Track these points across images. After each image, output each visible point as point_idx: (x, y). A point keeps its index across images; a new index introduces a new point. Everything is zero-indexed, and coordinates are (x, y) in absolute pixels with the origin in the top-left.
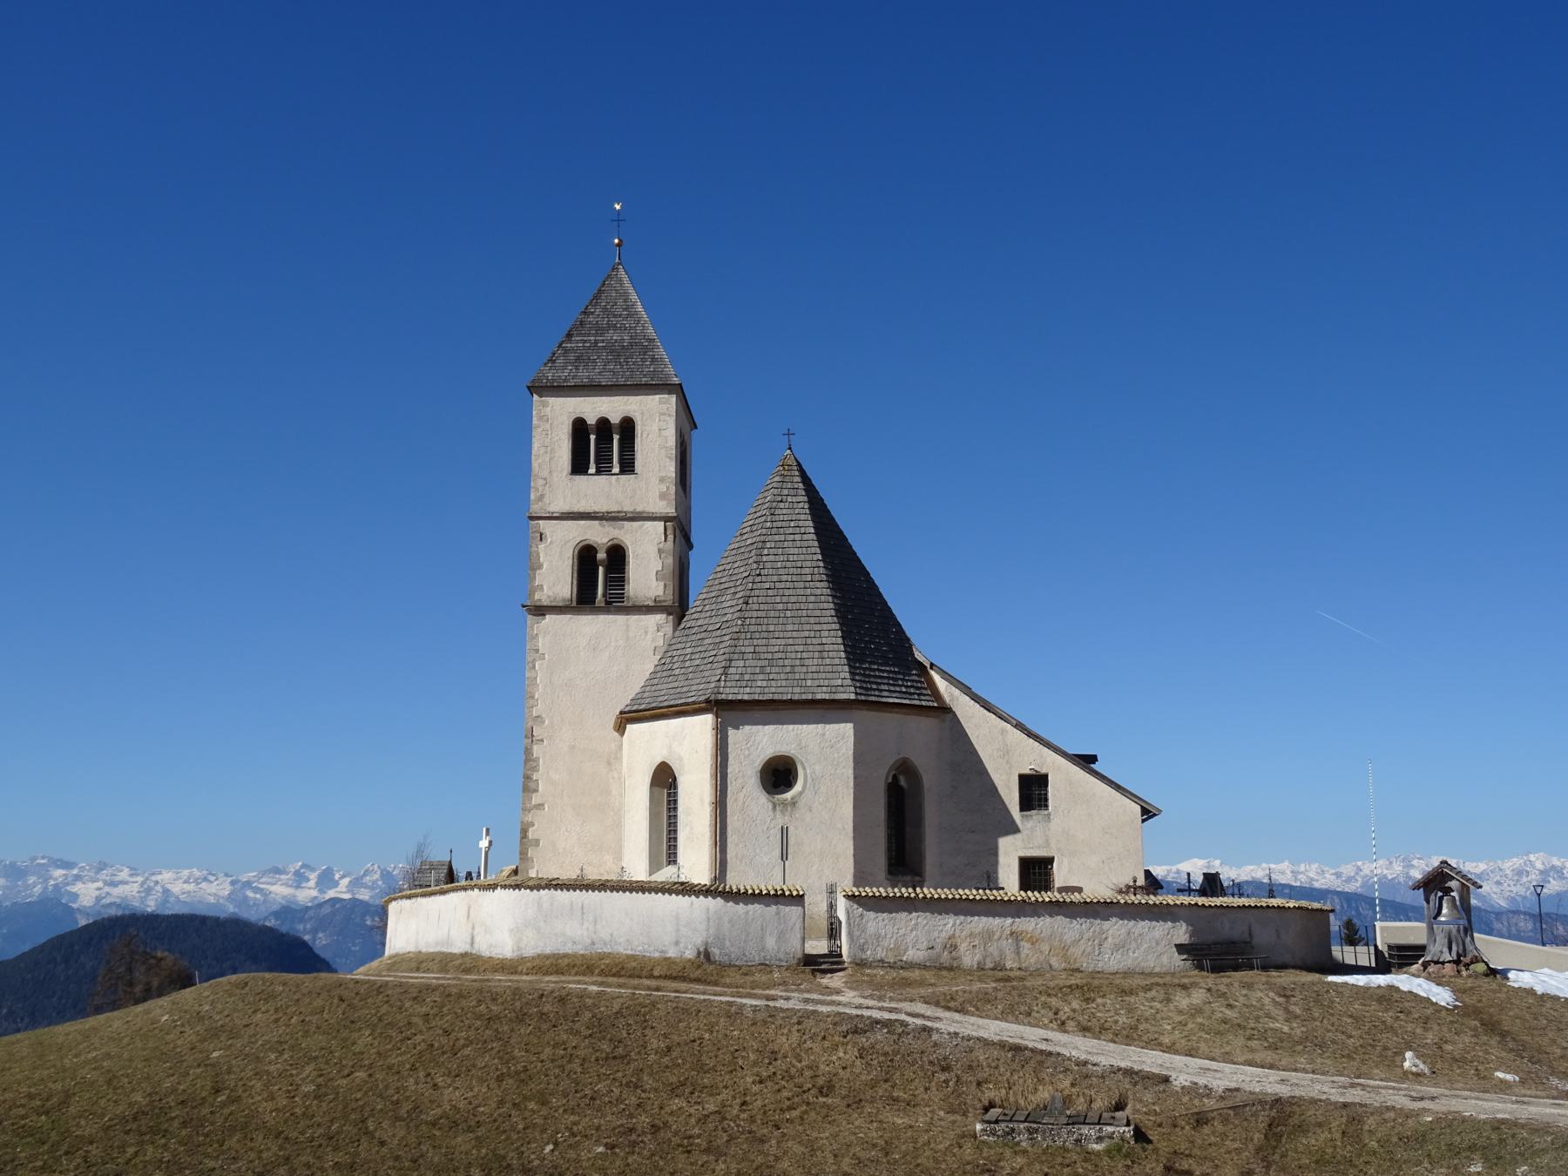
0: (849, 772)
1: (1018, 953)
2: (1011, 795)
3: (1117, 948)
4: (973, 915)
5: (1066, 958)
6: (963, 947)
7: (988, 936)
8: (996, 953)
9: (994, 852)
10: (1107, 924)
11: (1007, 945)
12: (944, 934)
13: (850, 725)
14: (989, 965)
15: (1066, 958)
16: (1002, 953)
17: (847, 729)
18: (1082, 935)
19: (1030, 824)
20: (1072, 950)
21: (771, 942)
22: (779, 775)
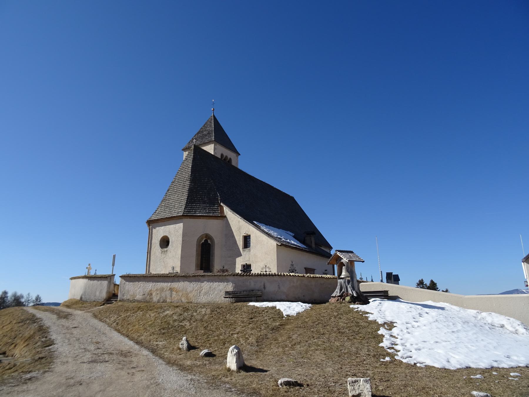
0: (181, 239)
1: (171, 296)
2: (240, 243)
3: (206, 293)
4: (158, 282)
5: (187, 298)
6: (154, 294)
7: (162, 290)
8: (164, 296)
9: (235, 264)
10: (203, 284)
11: (168, 293)
12: (148, 290)
13: (182, 224)
14: (162, 301)
15: (187, 298)
16: (166, 297)
17: (181, 225)
18: (193, 289)
19: (245, 253)
20: (190, 295)
21: (98, 293)
22: (165, 242)
